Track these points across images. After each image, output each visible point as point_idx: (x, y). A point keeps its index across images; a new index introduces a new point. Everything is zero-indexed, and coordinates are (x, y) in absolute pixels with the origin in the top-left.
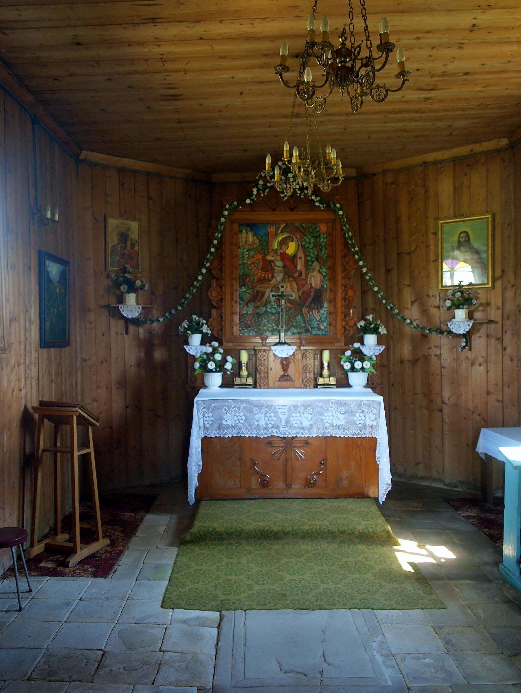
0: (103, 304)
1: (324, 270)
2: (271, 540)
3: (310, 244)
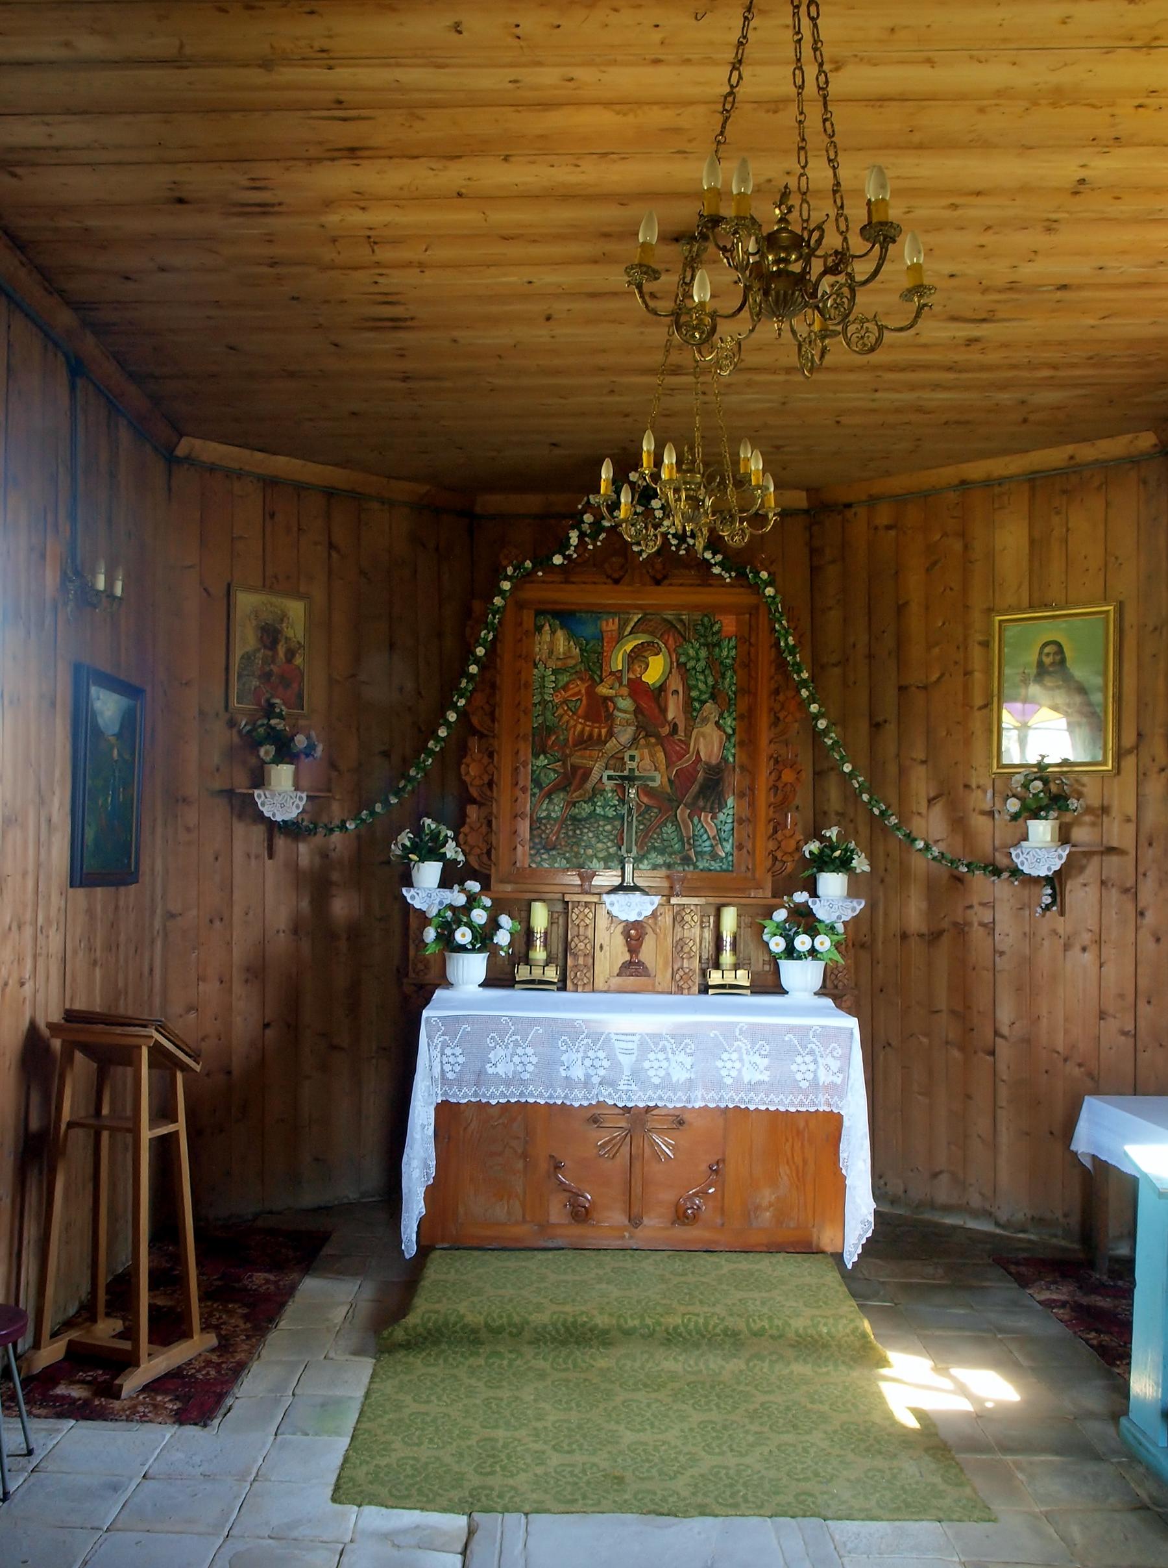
1: (729, 721)
2: (591, 1347)
3: (698, 660)
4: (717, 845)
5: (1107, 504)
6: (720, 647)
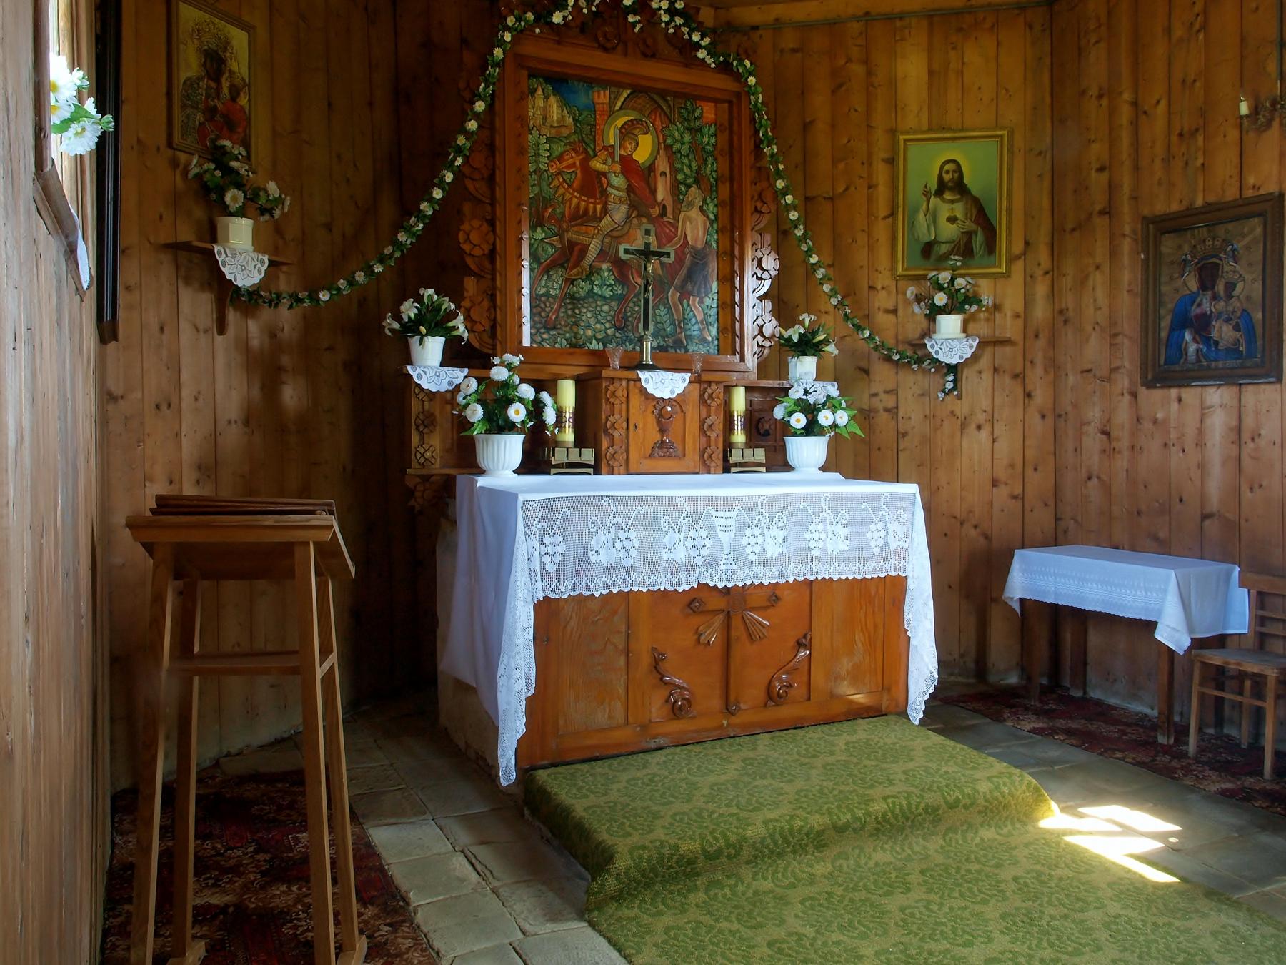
0: (163, 242)
1: (711, 207)
2: (807, 853)
3: (683, 144)
4: (704, 328)
5: (998, 44)
6: (701, 132)
